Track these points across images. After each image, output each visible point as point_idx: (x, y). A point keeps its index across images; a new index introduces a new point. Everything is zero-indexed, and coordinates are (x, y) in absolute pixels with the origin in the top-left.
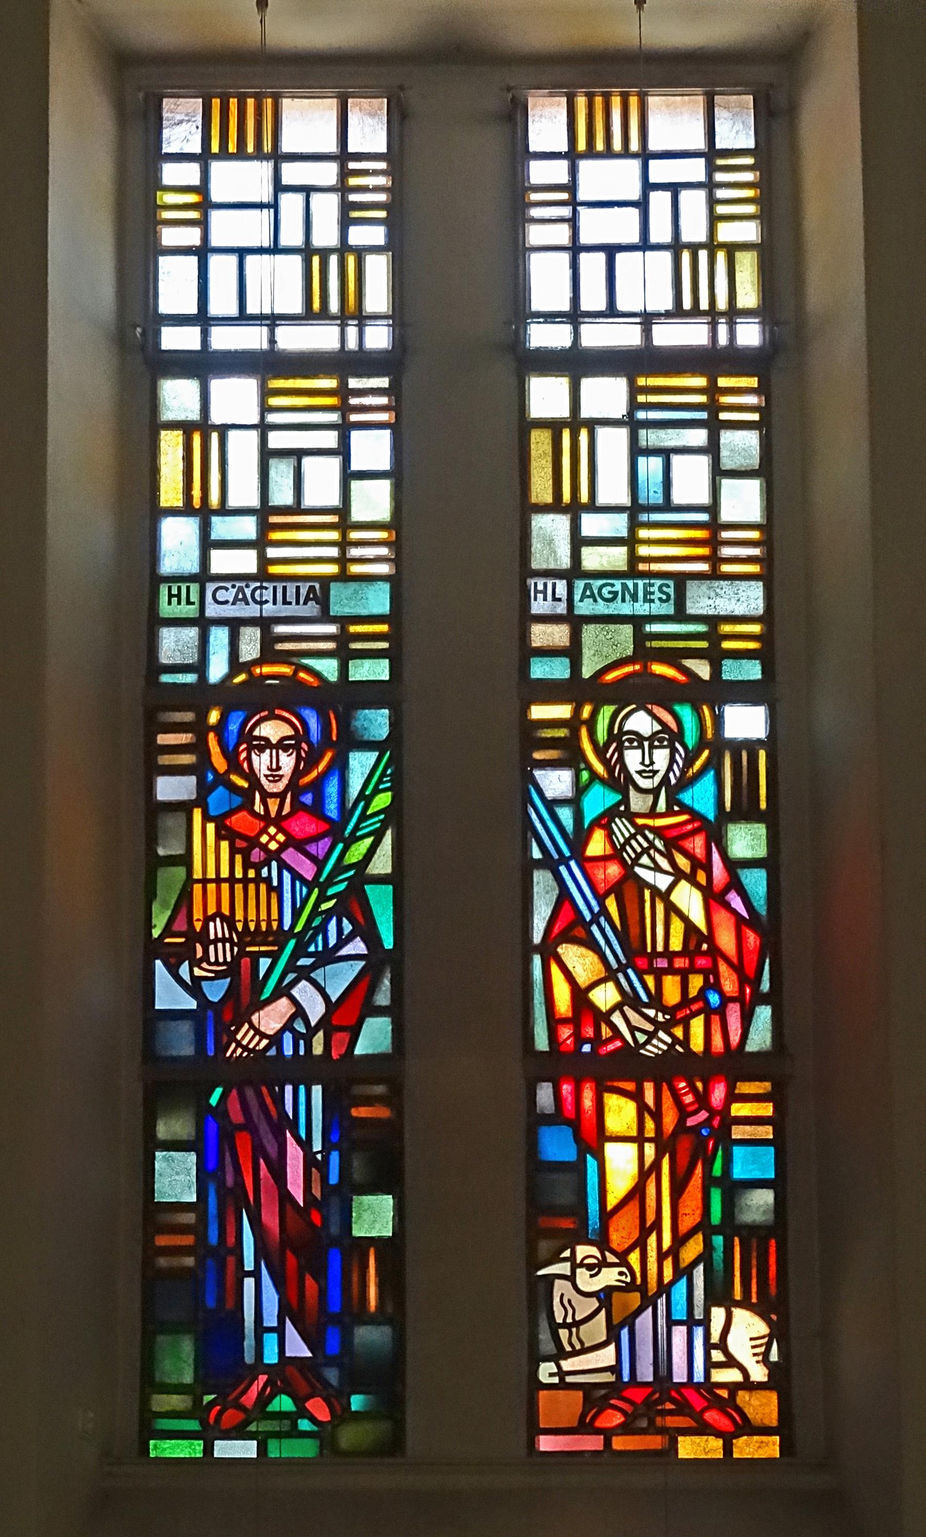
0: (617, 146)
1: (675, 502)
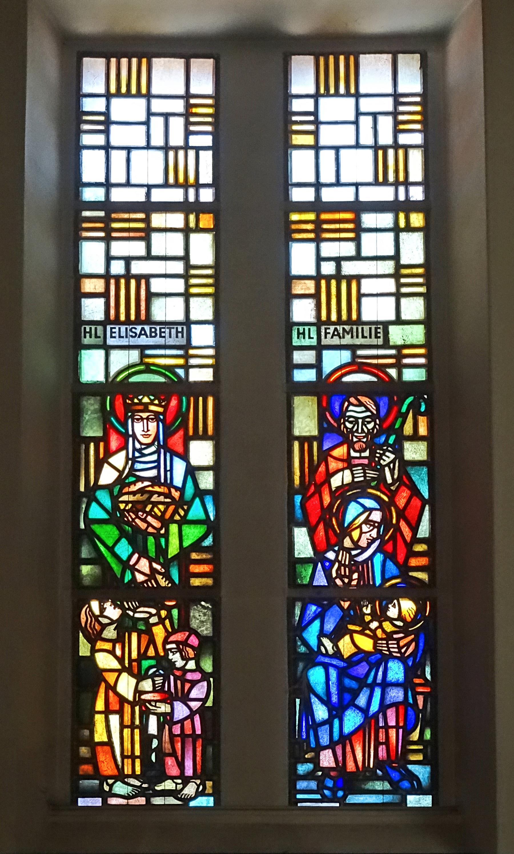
0: (134, 91)
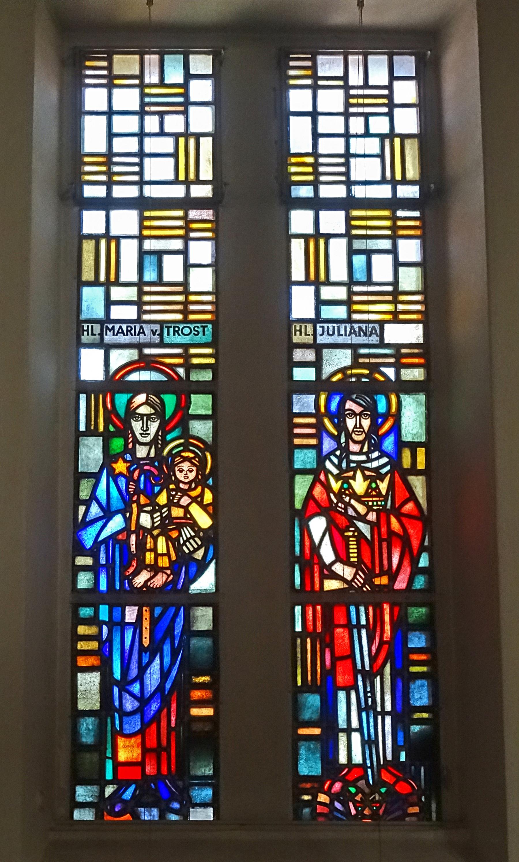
1: (182, 280)
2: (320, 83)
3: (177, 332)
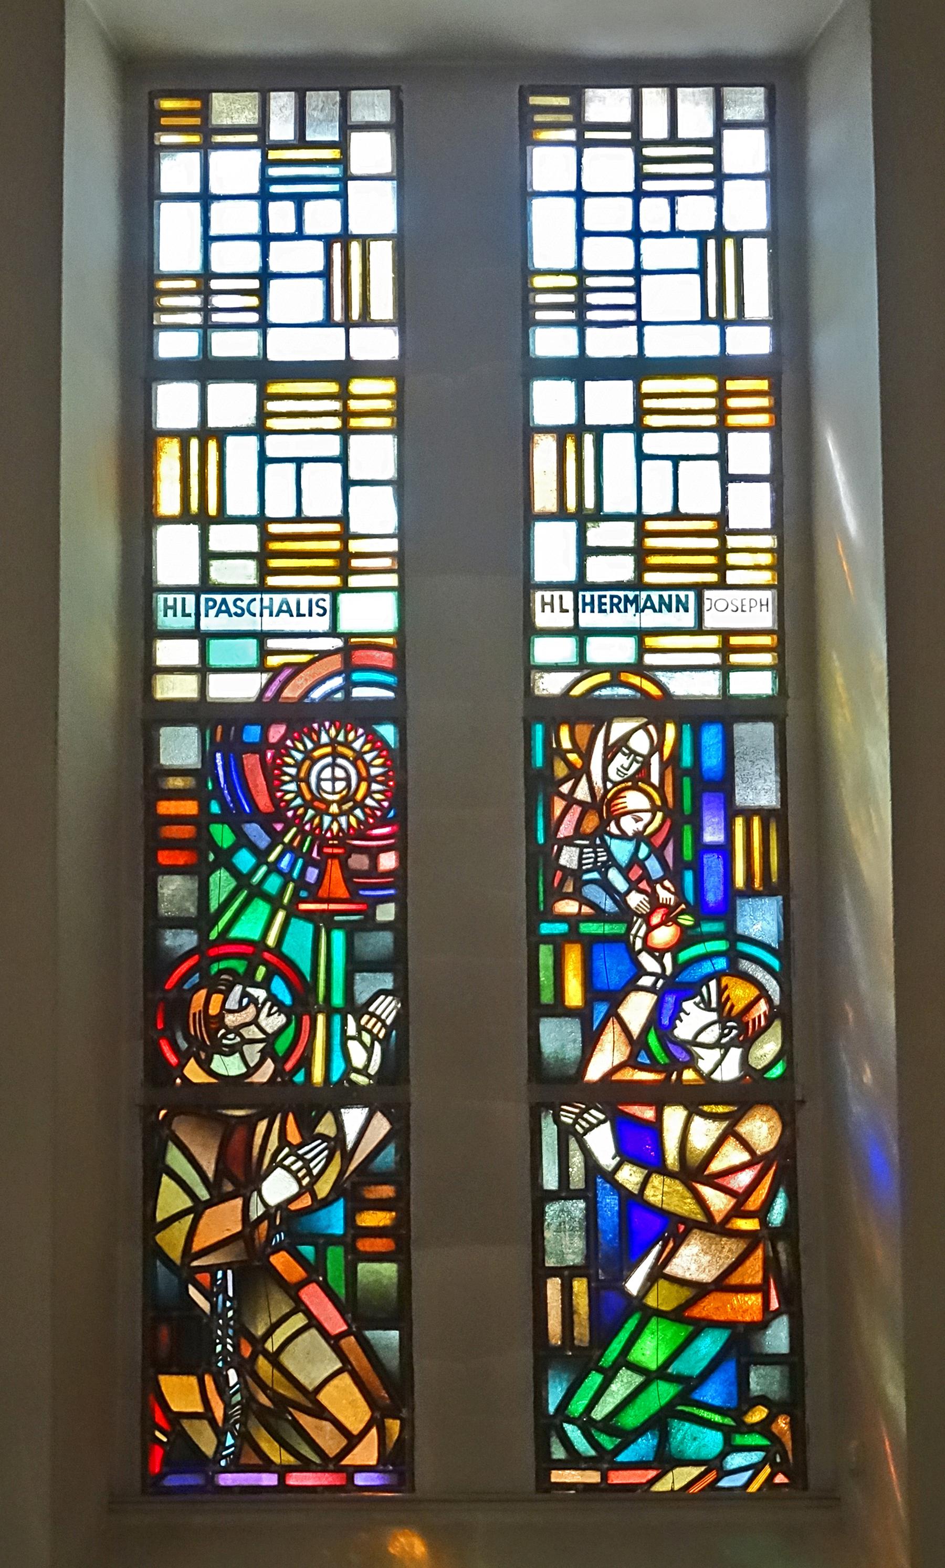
2: (589, 135)
3: (617, 605)
